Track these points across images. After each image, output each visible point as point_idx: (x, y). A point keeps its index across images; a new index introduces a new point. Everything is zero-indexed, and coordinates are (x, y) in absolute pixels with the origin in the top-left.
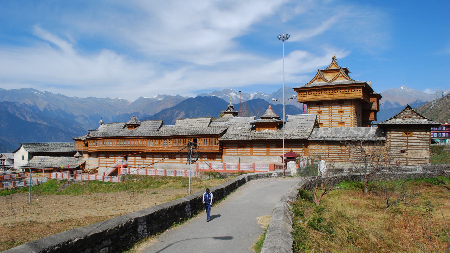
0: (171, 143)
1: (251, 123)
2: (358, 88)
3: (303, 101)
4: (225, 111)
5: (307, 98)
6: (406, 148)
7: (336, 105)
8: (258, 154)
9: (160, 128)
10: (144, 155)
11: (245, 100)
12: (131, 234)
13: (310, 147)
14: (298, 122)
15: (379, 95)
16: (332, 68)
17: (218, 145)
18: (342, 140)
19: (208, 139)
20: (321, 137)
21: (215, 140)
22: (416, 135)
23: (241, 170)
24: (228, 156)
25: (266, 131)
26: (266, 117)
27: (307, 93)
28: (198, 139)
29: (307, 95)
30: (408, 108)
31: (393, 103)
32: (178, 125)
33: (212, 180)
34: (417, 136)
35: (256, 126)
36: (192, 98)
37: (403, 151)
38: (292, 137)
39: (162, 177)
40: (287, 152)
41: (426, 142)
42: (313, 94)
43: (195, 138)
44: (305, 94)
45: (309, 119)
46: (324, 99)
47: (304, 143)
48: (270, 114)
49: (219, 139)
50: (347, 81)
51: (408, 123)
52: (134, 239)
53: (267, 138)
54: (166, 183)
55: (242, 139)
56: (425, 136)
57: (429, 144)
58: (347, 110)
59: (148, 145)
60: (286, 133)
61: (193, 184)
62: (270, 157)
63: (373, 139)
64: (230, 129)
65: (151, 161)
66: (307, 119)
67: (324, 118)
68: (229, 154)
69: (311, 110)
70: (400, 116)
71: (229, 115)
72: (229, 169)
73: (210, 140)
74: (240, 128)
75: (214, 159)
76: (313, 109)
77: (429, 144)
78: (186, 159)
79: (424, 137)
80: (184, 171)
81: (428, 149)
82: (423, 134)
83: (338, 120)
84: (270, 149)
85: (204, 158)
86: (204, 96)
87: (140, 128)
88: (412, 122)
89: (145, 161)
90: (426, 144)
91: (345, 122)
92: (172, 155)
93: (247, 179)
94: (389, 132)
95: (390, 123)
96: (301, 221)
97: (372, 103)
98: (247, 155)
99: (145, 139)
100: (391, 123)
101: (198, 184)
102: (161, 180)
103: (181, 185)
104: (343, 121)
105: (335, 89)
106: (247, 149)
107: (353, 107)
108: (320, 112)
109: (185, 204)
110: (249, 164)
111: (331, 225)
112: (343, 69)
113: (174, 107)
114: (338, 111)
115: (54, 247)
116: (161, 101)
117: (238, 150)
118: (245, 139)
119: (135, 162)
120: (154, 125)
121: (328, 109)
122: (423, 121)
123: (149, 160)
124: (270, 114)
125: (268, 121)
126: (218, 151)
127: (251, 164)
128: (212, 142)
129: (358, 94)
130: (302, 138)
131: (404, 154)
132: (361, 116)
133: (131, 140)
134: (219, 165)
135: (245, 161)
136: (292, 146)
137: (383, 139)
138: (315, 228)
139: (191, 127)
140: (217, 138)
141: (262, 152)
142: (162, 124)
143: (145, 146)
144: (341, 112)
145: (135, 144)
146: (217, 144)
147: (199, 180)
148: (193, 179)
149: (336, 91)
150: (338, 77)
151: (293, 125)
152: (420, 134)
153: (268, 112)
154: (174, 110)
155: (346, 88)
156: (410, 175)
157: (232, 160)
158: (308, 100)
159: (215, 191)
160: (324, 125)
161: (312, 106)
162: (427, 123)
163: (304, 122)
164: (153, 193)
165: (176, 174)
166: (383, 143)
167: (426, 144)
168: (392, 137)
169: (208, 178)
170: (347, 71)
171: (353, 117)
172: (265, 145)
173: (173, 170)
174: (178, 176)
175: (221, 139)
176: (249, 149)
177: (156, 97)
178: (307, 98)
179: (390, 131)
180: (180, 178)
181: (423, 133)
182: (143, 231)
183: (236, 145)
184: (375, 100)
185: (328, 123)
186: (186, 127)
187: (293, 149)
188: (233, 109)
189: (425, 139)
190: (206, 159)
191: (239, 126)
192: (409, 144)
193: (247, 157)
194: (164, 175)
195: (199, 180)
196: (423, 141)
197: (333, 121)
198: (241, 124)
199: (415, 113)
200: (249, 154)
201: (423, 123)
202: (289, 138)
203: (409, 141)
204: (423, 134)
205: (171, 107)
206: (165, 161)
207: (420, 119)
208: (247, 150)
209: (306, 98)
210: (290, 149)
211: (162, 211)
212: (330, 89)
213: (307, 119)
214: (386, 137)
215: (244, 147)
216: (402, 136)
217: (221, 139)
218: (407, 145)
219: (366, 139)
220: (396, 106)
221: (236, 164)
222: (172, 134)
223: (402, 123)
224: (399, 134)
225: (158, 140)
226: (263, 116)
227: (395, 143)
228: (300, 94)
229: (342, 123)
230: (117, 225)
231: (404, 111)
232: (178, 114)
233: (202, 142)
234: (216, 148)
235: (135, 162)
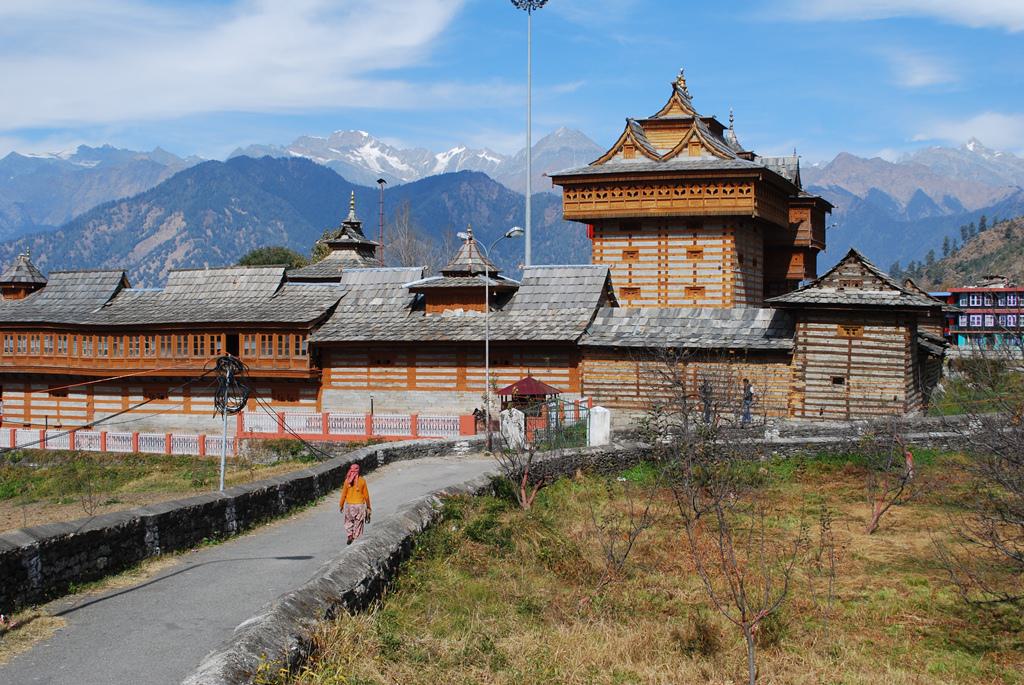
0: (153, 347)
1: (412, 290)
2: (742, 182)
3: (581, 215)
4: (332, 240)
5: (593, 207)
6: (845, 371)
7: (680, 233)
8: (431, 385)
9: (114, 296)
10: (59, 384)
11: (416, 177)
12: (136, 543)
13: (587, 365)
14: (553, 289)
15: (819, 200)
16: (669, 116)
17: (307, 357)
18: (675, 345)
19: (275, 337)
20: (618, 336)
21: (297, 339)
22: (873, 334)
23: (376, 433)
24: (339, 392)
25: (455, 313)
26: (458, 269)
27: (594, 193)
28: (242, 337)
29: (594, 198)
30: (852, 259)
31: (938, 201)
32: (176, 289)
33: (285, 465)
34: (873, 336)
35: (424, 298)
36: (213, 164)
37: (838, 381)
38: (535, 336)
39: (125, 457)
40: (518, 379)
41: (895, 353)
42: (609, 197)
43: (232, 332)
44: (586, 194)
45: (586, 281)
46: (641, 214)
47: (567, 353)
48: (470, 261)
49: (310, 338)
50: (714, 158)
51: (850, 301)
52: (141, 555)
53: (458, 337)
54: (139, 476)
55: (382, 338)
56: (893, 337)
57: (903, 362)
58: (714, 250)
59: (75, 355)
60: (521, 320)
61: (229, 477)
62: (466, 394)
63: (760, 344)
64: (346, 305)
65: (84, 405)
66: (579, 281)
67: (643, 273)
68: (340, 384)
69: (605, 244)
70: (831, 280)
71: (344, 253)
72: (339, 432)
73: (280, 339)
74: (377, 301)
75: (292, 400)
76: (612, 244)
77: (903, 362)
78: (212, 399)
79: (891, 341)
80: (195, 436)
81: (902, 374)
82: (889, 333)
83: (686, 280)
84: (468, 370)
85: (261, 396)
86: (261, 155)
87: (46, 293)
88: (860, 296)
89: (63, 404)
90: (895, 361)
91: (707, 287)
92: (156, 387)
93: (381, 457)
94: (802, 326)
95: (802, 301)
96: (454, 528)
97: (798, 225)
98: (398, 389)
99: (64, 332)
100: (807, 299)
101: (242, 478)
102: (121, 467)
103: (188, 482)
104: (700, 282)
105: (677, 183)
106: (396, 370)
107: (728, 241)
108: (631, 254)
109: (224, 504)
110: (400, 416)
111: (509, 533)
112: (704, 120)
113: (144, 194)
114: (684, 251)
115: (51, 538)
116: (91, 171)
117: (369, 373)
118: (392, 338)
119: (27, 407)
120: (94, 287)
121: (655, 243)
122: (890, 297)
123: (76, 401)
124: (470, 261)
125: (463, 282)
126: (308, 376)
127: (407, 416)
128: (287, 346)
129: (744, 202)
130: (563, 338)
131: (841, 389)
132: (759, 266)
133: (15, 335)
134: (309, 420)
135: (392, 408)
136: (531, 361)
137: (787, 343)
138: (476, 539)
139: (220, 294)
140: (305, 333)
141: (443, 378)
142: (123, 283)
143: (65, 355)
144: (695, 253)
145: (29, 349)
146: (304, 353)
147: (244, 465)
148: (231, 462)
149: (680, 190)
150: (686, 146)
151: (541, 298)
152: (883, 333)
153: (465, 254)
154: (144, 208)
155: (709, 182)
156: (824, 445)
157: (349, 404)
158: (595, 215)
159: (292, 482)
160: (643, 295)
161: (609, 234)
162: (897, 302)
163: (570, 289)
164: (109, 503)
165: (170, 449)
166: (784, 356)
167: (895, 361)
168: (810, 340)
169: (275, 459)
170: (716, 128)
171: (728, 271)
172: (453, 357)
173: (162, 435)
174: (175, 452)
175: (315, 337)
176: (405, 370)
177: (73, 156)
178: (593, 207)
179: (806, 322)
180: (184, 460)
181: (889, 329)
182: (153, 543)
183: (365, 356)
184: (806, 214)
185: (656, 288)
186: (203, 296)
187: (533, 371)
188: (361, 234)
189: (894, 345)
190: (269, 400)
191: (373, 295)
192: (853, 358)
193: (399, 394)
194: (130, 450)
195: (244, 465)
196: (889, 353)
197: (670, 280)
198: (382, 290)
199: (870, 271)
200: (405, 385)
201: (887, 302)
202: (525, 338)
203: (854, 351)
204: (889, 333)
205: (132, 195)
206: (194, 408)
207: (881, 289)
208: (399, 373)
209: (589, 207)
210: (525, 371)
211: (182, 511)
212: (662, 184)
213: (579, 281)
214: (796, 340)
215: (388, 363)
216: (836, 337)
217: (315, 337)
218: (849, 362)
219: (741, 343)
220: (948, 212)
221: (362, 416)
222: (156, 317)
223: (834, 301)
224: (829, 330)
225: (110, 338)
226: (450, 268)
227: (819, 357)
228: (572, 194)
229: (695, 289)
230: (117, 524)
231: (840, 265)
232: (160, 221)
233: (254, 346)
234: (300, 365)
235: (27, 407)
